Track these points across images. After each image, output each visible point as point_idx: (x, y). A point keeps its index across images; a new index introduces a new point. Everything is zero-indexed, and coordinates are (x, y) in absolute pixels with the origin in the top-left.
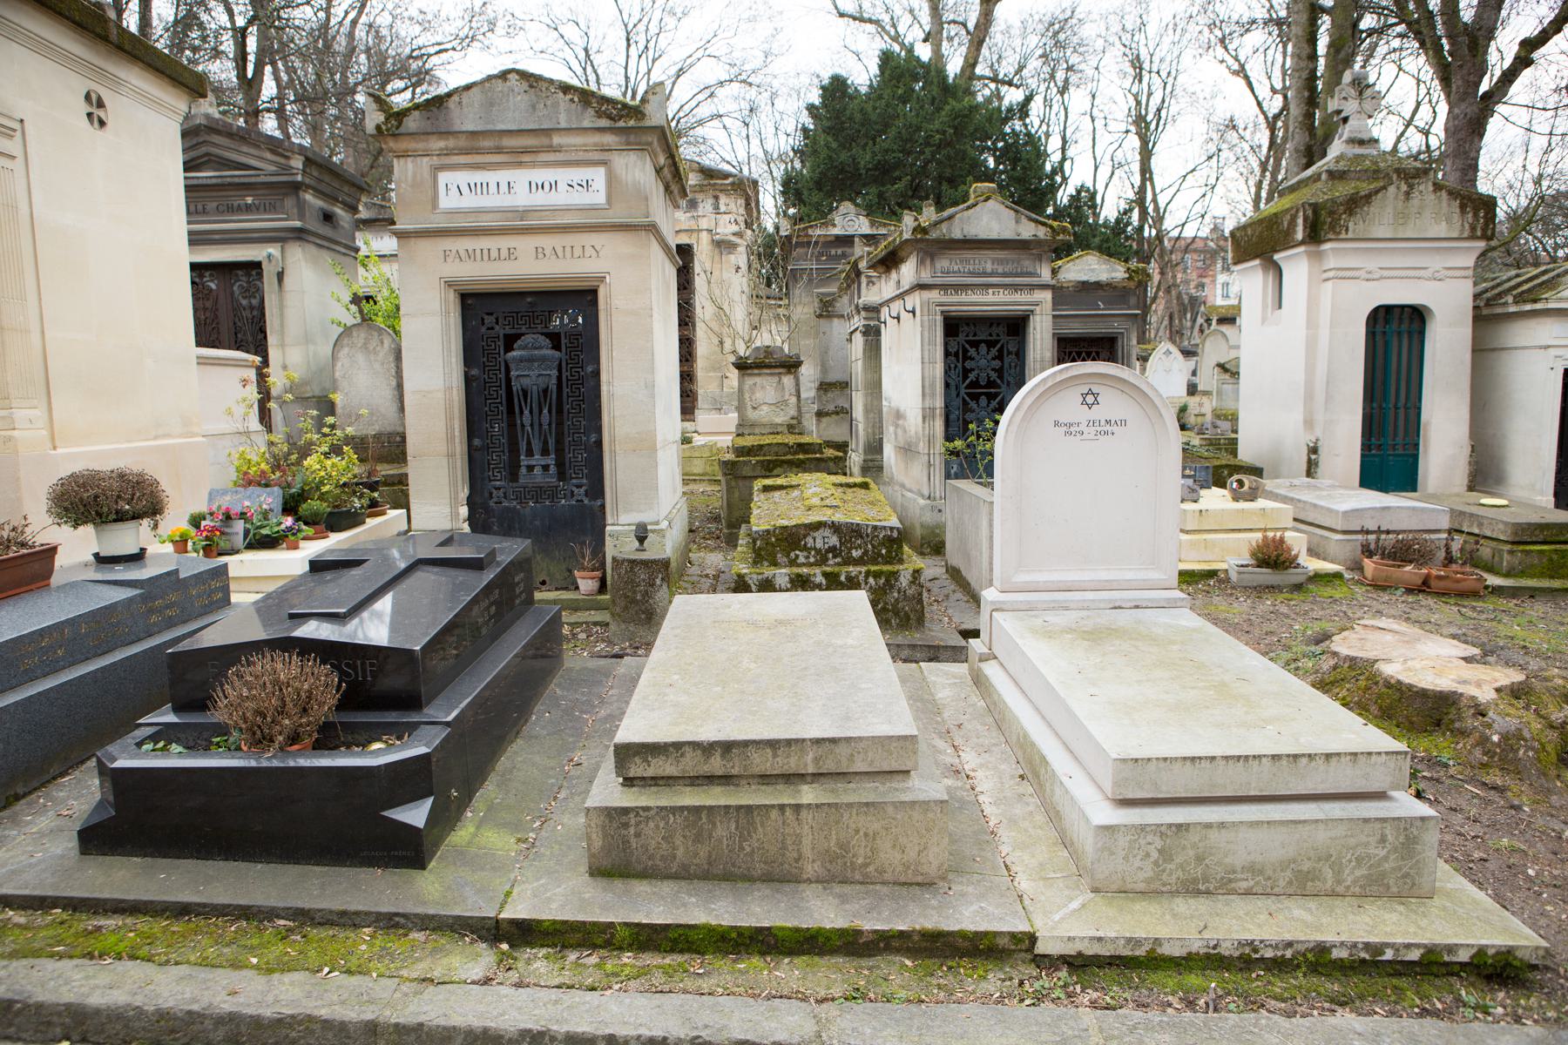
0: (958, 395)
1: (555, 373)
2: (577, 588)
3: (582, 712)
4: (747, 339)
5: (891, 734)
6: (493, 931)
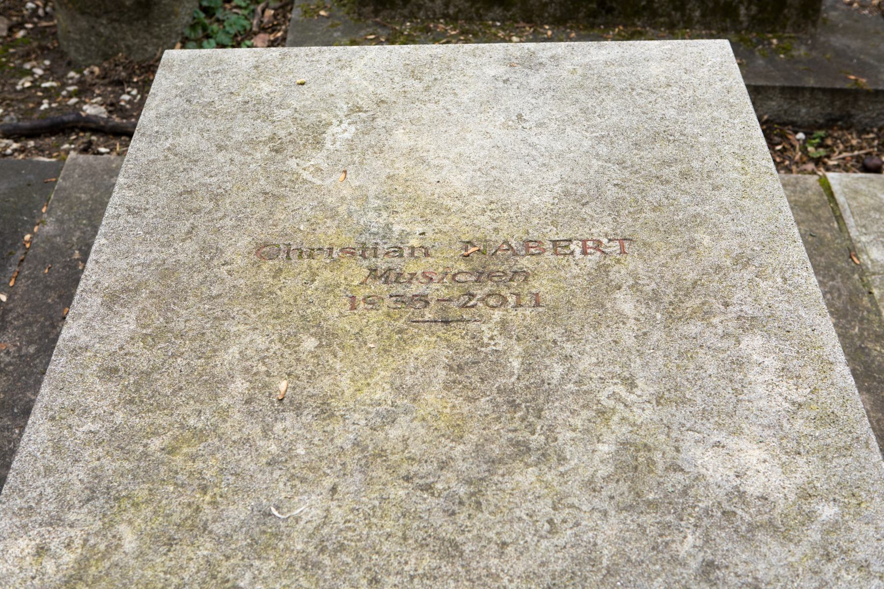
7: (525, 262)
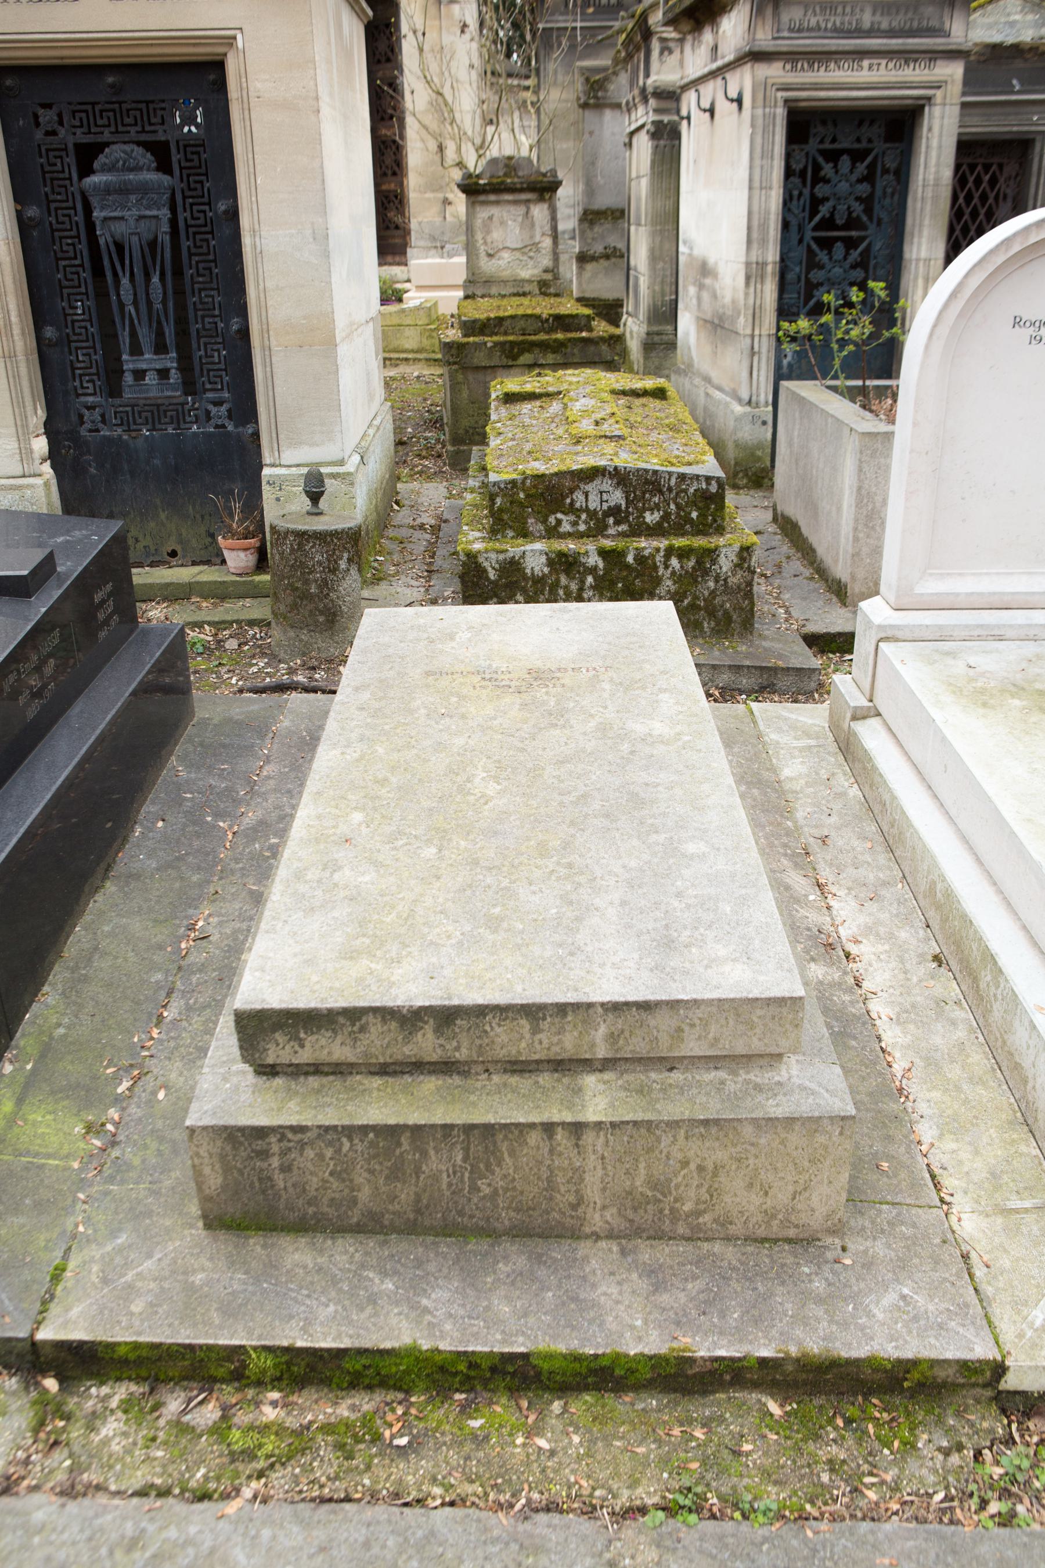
0: (801, 241)
1: (165, 213)
2: (224, 562)
3: (219, 815)
4: (478, 141)
5: (755, 993)
6: (29, 1357)
7: (558, 675)
